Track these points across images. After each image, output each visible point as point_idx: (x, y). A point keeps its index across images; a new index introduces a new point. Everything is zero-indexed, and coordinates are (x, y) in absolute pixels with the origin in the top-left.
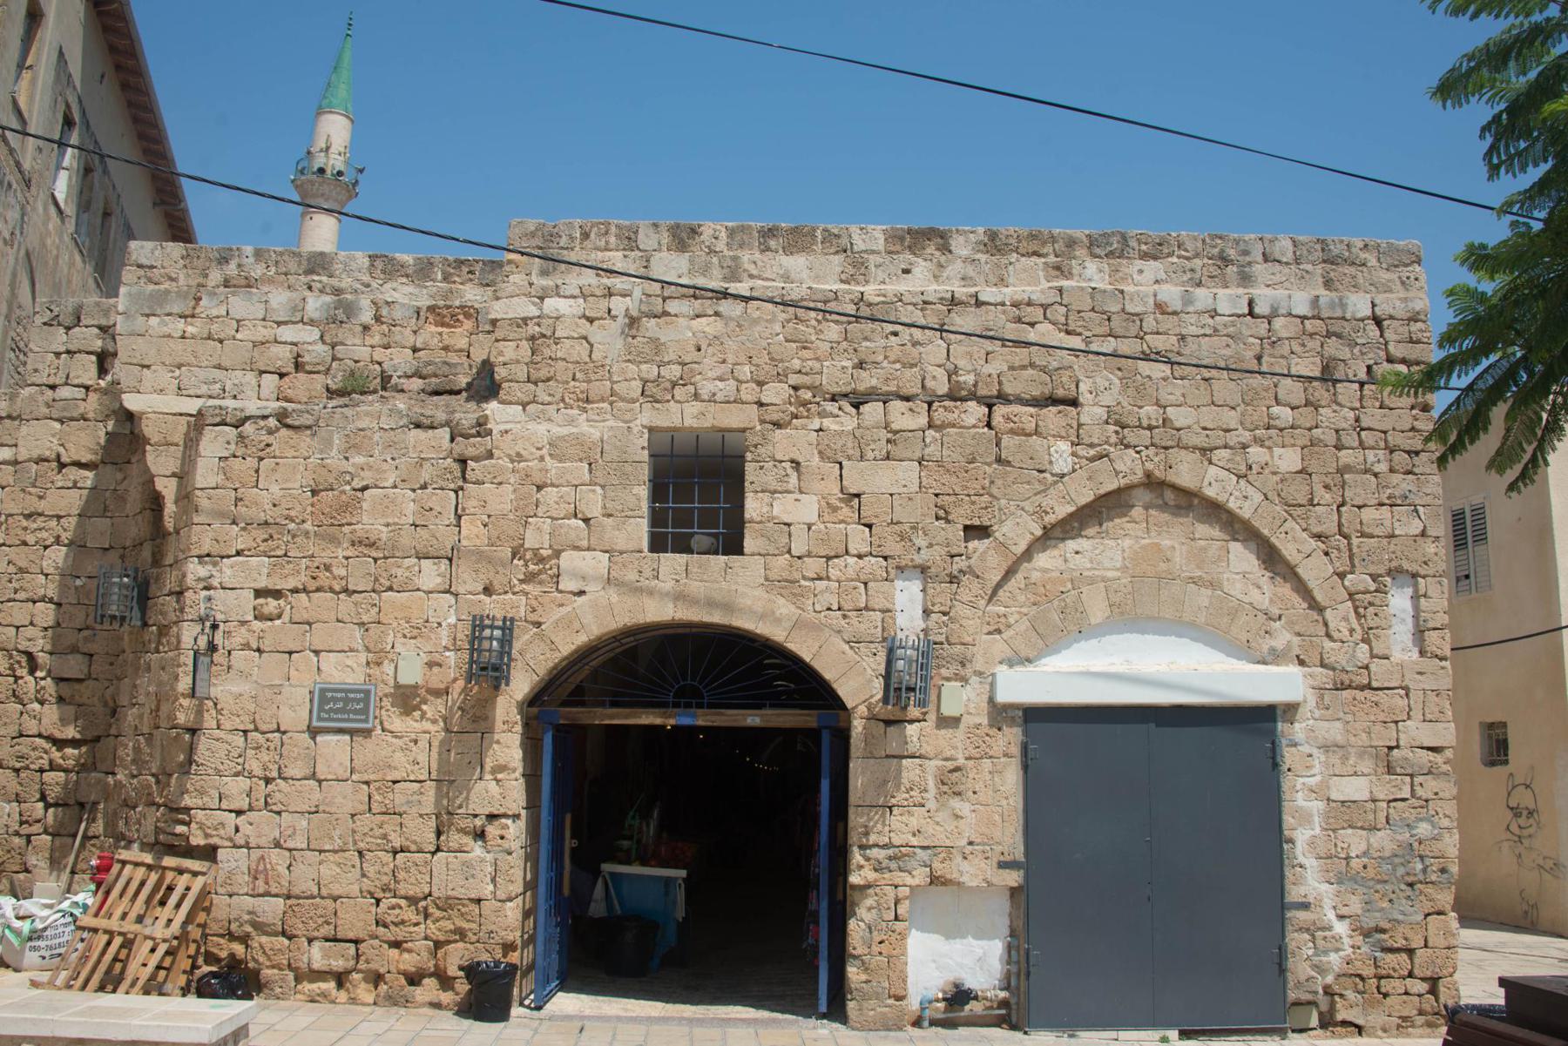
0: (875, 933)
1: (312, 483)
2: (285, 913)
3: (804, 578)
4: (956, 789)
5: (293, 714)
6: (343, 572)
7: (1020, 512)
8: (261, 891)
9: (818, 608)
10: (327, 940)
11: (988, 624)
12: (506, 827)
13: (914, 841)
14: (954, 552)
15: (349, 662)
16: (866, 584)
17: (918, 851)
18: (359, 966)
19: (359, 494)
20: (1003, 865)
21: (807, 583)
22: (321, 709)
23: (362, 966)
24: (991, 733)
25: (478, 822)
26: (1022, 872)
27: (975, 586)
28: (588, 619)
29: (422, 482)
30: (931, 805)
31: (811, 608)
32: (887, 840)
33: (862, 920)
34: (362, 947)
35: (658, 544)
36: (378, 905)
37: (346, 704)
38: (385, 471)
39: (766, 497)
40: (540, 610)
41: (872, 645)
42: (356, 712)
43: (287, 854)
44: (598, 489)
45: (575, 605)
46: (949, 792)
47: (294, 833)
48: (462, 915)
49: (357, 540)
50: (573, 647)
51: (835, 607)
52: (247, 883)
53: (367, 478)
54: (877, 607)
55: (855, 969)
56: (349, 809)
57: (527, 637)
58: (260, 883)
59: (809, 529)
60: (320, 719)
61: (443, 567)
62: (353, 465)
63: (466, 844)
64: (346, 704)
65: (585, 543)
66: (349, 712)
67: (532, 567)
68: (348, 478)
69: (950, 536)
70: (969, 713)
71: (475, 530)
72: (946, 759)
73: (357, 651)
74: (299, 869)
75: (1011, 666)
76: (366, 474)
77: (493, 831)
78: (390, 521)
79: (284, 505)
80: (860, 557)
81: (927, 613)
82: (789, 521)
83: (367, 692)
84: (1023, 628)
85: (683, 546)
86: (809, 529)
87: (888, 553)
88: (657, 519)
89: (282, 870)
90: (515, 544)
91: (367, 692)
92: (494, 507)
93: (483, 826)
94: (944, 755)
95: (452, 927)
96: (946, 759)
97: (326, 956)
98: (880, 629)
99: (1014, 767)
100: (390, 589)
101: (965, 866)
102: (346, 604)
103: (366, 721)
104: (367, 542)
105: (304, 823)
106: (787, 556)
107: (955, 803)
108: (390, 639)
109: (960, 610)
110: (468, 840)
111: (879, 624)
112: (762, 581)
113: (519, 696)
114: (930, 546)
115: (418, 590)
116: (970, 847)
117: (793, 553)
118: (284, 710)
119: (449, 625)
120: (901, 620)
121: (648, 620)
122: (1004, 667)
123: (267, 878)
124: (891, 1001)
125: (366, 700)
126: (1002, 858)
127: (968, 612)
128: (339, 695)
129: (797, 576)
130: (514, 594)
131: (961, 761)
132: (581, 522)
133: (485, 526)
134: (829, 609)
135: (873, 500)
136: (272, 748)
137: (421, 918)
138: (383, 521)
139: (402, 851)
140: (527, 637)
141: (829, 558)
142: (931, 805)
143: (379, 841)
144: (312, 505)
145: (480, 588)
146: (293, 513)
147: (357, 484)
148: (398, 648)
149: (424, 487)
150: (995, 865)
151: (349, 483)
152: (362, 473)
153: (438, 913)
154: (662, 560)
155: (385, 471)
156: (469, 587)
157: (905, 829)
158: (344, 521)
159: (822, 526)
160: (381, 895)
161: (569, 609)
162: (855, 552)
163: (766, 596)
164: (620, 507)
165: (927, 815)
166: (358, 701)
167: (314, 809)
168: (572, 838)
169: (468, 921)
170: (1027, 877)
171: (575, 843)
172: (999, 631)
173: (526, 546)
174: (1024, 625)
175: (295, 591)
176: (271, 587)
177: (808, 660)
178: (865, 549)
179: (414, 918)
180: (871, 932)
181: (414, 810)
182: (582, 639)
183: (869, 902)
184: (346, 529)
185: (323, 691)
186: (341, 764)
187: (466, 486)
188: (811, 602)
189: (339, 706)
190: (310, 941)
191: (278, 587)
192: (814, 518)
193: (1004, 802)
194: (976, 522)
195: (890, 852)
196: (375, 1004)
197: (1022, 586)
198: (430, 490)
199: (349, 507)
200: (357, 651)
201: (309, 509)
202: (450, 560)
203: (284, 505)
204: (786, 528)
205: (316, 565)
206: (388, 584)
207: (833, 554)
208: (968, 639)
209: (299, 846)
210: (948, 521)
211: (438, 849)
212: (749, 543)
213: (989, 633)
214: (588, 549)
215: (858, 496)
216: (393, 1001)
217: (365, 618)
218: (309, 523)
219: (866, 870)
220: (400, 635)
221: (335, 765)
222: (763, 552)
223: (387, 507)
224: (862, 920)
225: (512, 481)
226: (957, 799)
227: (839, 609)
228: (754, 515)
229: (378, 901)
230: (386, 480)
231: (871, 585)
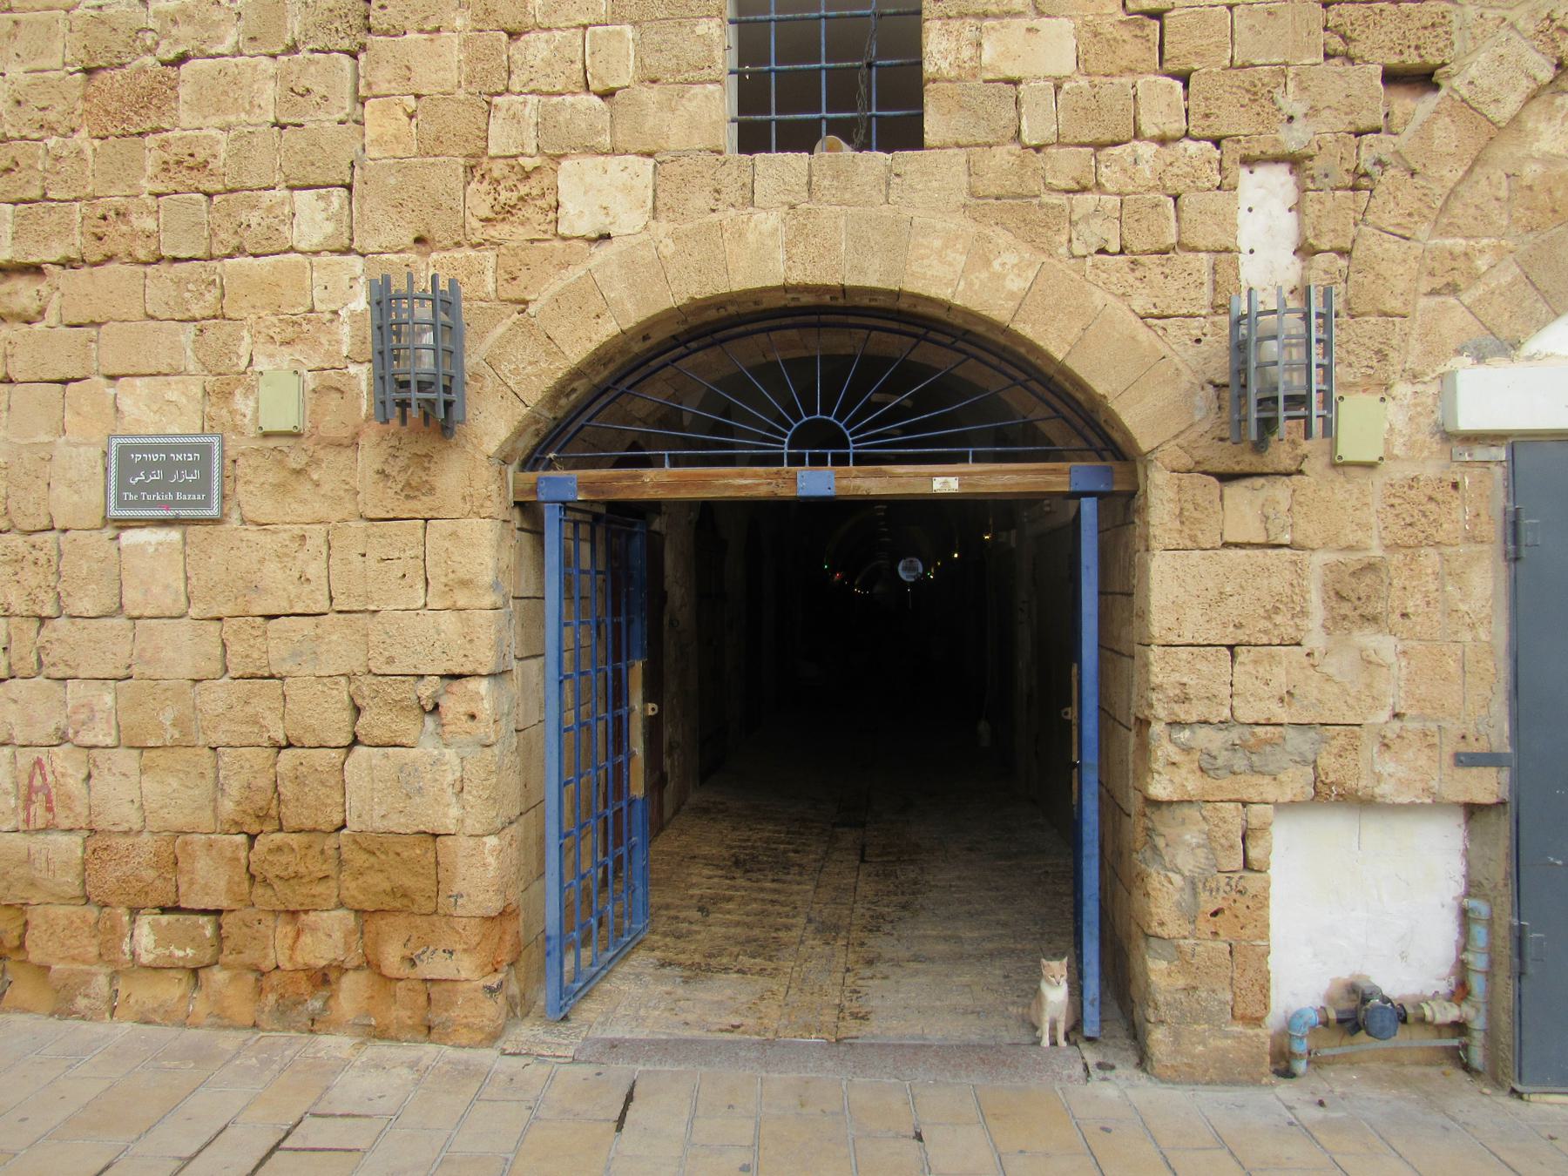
0: (1204, 896)
1: (82, 55)
2: (84, 862)
3: (1051, 189)
4: (1369, 611)
5: (76, 498)
6: (149, 224)
7: (1504, 33)
8: (40, 824)
9: (1079, 249)
10: (164, 910)
11: (1432, 274)
12: (476, 697)
13: (1282, 715)
14: (1363, 124)
15: (172, 395)
16: (1176, 198)
17: (1290, 733)
18: (222, 958)
19: (171, 72)
20: (1465, 760)
21: (1055, 199)
22: (123, 485)
23: (228, 957)
24: (1439, 497)
25: (426, 690)
26: (1505, 775)
27: (1408, 197)
28: (617, 291)
29: (288, 40)
30: (1315, 639)
31: (1063, 250)
32: (1226, 713)
33: (1178, 871)
34: (226, 919)
35: (752, 140)
36: (251, 847)
37: (168, 475)
38: (217, 24)
39: (967, 29)
40: (524, 277)
41: (1194, 323)
42: (187, 488)
43: (82, 755)
44: (628, 30)
45: (592, 264)
46: (1354, 615)
47: (92, 719)
48: (404, 862)
49: (172, 159)
50: (592, 347)
51: (1114, 247)
52: (15, 810)
53: (185, 38)
54: (1201, 244)
55: (1163, 964)
56: (186, 669)
57: (500, 330)
58: (38, 809)
59: (1058, 88)
60: (121, 503)
61: (336, 202)
62: (157, 14)
63: (405, 733)
64: (168, 475)
65: (605, 141)
66: (175, 488)
67: (504, 196)
68: (149, 39)
69: (1356, 89)
70: (1395, 458)
71: (391, 128)
72: (1350, 548)
73: (186, 373)
74: (105, 784)
75: (1480, 359)
76: (183, 31)
77: (453, 706)
78: (232, 119)
79: (33, 103)
80: (1163, 141)
81: (1305, 251)
82: (1015, 74)
83: (206, 450)
84: (1506, 279)
85: (800, 139)
86: (1058, 88)
87: (1224, 131)
88: (750, 96)
89: (74, 783)
90: (471, 149)
91: (206, 450)
92: (425, 79)
93: (435, 695)
94: (1343, 544)
95: (387, 886)
96: (1350, 548)
97: (163, 938)
98: (1207, 289)
99: (1487, 563)
100: (240, 250)
101: (1387, 766)
102: (161, 286)
103: (206, 504)
104: (191, 162)
105: (109, 699)
106: (1016, 148)
107: (1368, 639)
108: (244, 349)
109: (1372, 244)
110: (407, 727)
111: (1206, 278)
112: (963, 197)
113: (492, 446)
114: (1314, 111)
115: (292, 249)
116: (1396, 724)
117: (1025, 137)
118: (61, 491)
119: (353, 314)
120: (1252, 272)
121: (736, 288)
122: (1466, 360)
123: (49, 800)
124: (1238, 1028)
125: (205, 464)
126: (1462, 748)
127: (1392, 246)
128: (155, 457)
129: (1034, 186)
130: (475, 246)
131: (1376, 552)
132: (596, 99)
133: (411, 117)
134: (1102, 251)
135: (1189, 19)
136: (43, 560)
137: (329, 868)
138: (217, 120)
139: (290, 745)
140: (500, 330)
141: (1099, 146)
142: (1315, 639)
143: (244, 728)
144: (86, 98)
145: (408, 240)
146: (51, 116)
147: (168, 51)
148: (261, 364)
149: (293, 49)
150: (1447, 760)
151: (149, 51)
152: (174, 31)
153: (360, 859)
154: (760, 167)
155: (217, 24)
156: (385, 240)
157: (1264, 691)
158: (147, 126)
159: (1084, 82)
160: (255, 829)
161: (578, 272)
162: (1155, 132)
163: (973, 228)
164: (672, 64)
165: (1305, 660)
166: (190, 466)
167: (122, 673)
168: (646, 700)
169: (416, 874)
170: (1516, 786)
171: (652, 710)
172: (1453, 289)
173: (492, 151)
174: (1507, 275)
175: (67, 263)
176: (21, 259)
177: (1060, 357)
178: (1176, 126)
179: (319, 869)
180: (1195, 893)
181: (307, 669)
182: (608, 329)
183: (1192, 837)
184: (150, 141)
185: (124, 451)
186: (167, 587)
187: (372, 40)
188: (1064, 238)
189: (157, 476)
190: (134, 911)
191: (33, 259)
192: (1067, 66)
193: (1467, 636)
194: (1412, 59)
195: (1234, 735)
196: (255, 1025)
197: (1503, 194)
198: (304, 55)
199: (158, 96)
200: (186, 373)
201: (80, 106)
202: (349, 187)
203: (33, 103)
204: (1009, 88)
205: (99, 212)
206: (235, 242)
207: (1108, 137)
208: (1393, 304)
209: (102, 740)
210: (1351, 59)
211: (356, 741)
212: (934, 125)
213: (1434, 292)
214: (613, 152)
215: (1157, 15)
216: (285, 1010)
217: (196, 311)
218: (84, 133)
219: (1183, 771)
220: (261, 339)
221: (156, 590)
222: (963, 141)
223: (225, 93)
224: (1178, 871)
225: (459, 23)
226: (1369, 629)
227: (1122, 252)
228: (944, 65)
229: (252, 838)
230: (220, 40)
231: (1185, 201)
